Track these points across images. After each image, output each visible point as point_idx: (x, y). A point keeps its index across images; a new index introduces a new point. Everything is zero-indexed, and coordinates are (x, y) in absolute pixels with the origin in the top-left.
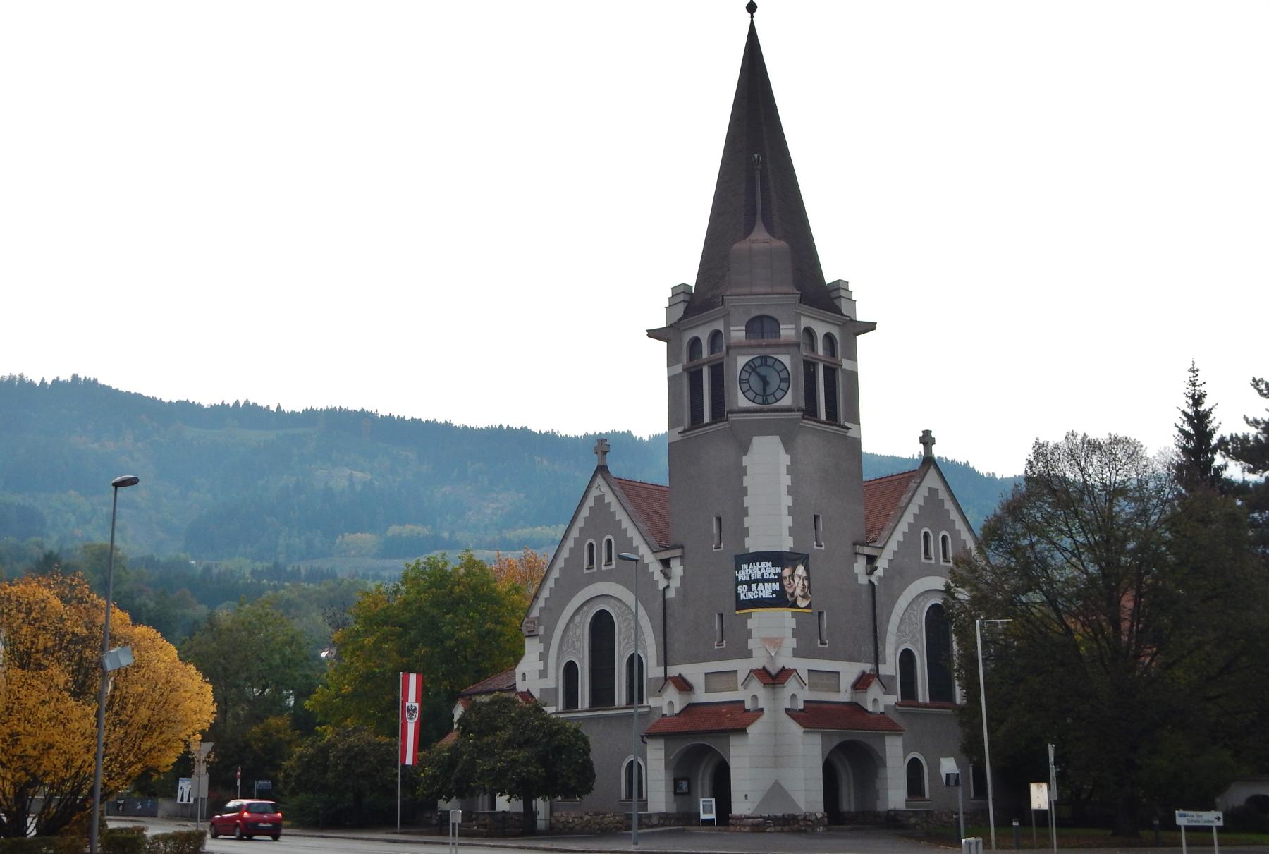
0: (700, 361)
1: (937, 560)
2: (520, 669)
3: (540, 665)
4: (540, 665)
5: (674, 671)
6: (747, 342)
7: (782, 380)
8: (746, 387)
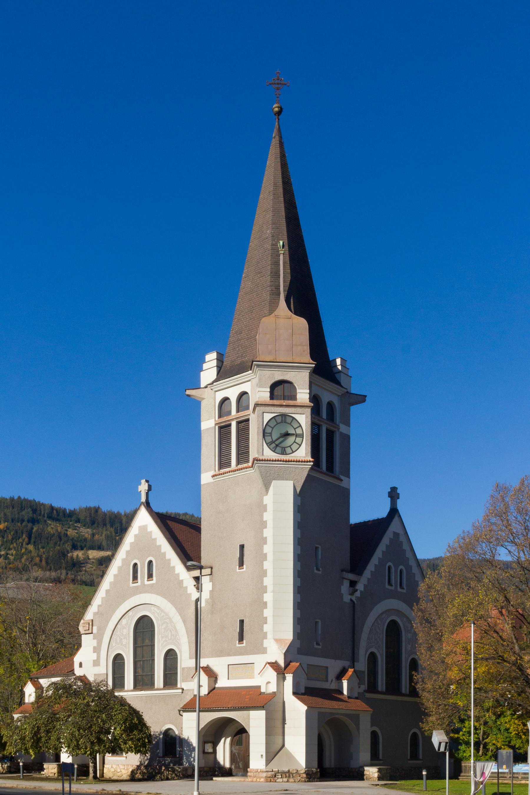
0: (230, 418)
1: (396, 587)
2: (77, 659)
3: (94, 656)
4: (94, 656)
5: (204, 662)
6: (272, 402)
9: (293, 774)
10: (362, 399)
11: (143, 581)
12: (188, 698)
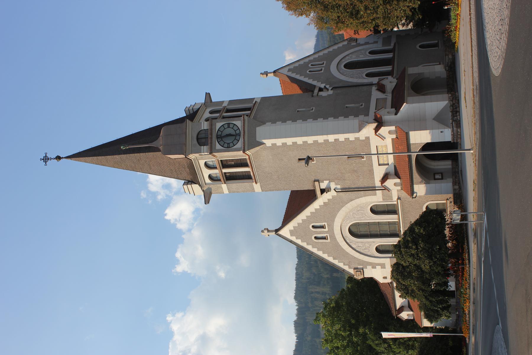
2: (381, 280)
3: (378, 267)
4: (378, 267)
5: (378, 184)
6: (209, 144)
7: (229, 127)
8: (231, 145)
9: (453, 109)
10: (208, 95)
11: (326, 232)
12: (404, 195)
